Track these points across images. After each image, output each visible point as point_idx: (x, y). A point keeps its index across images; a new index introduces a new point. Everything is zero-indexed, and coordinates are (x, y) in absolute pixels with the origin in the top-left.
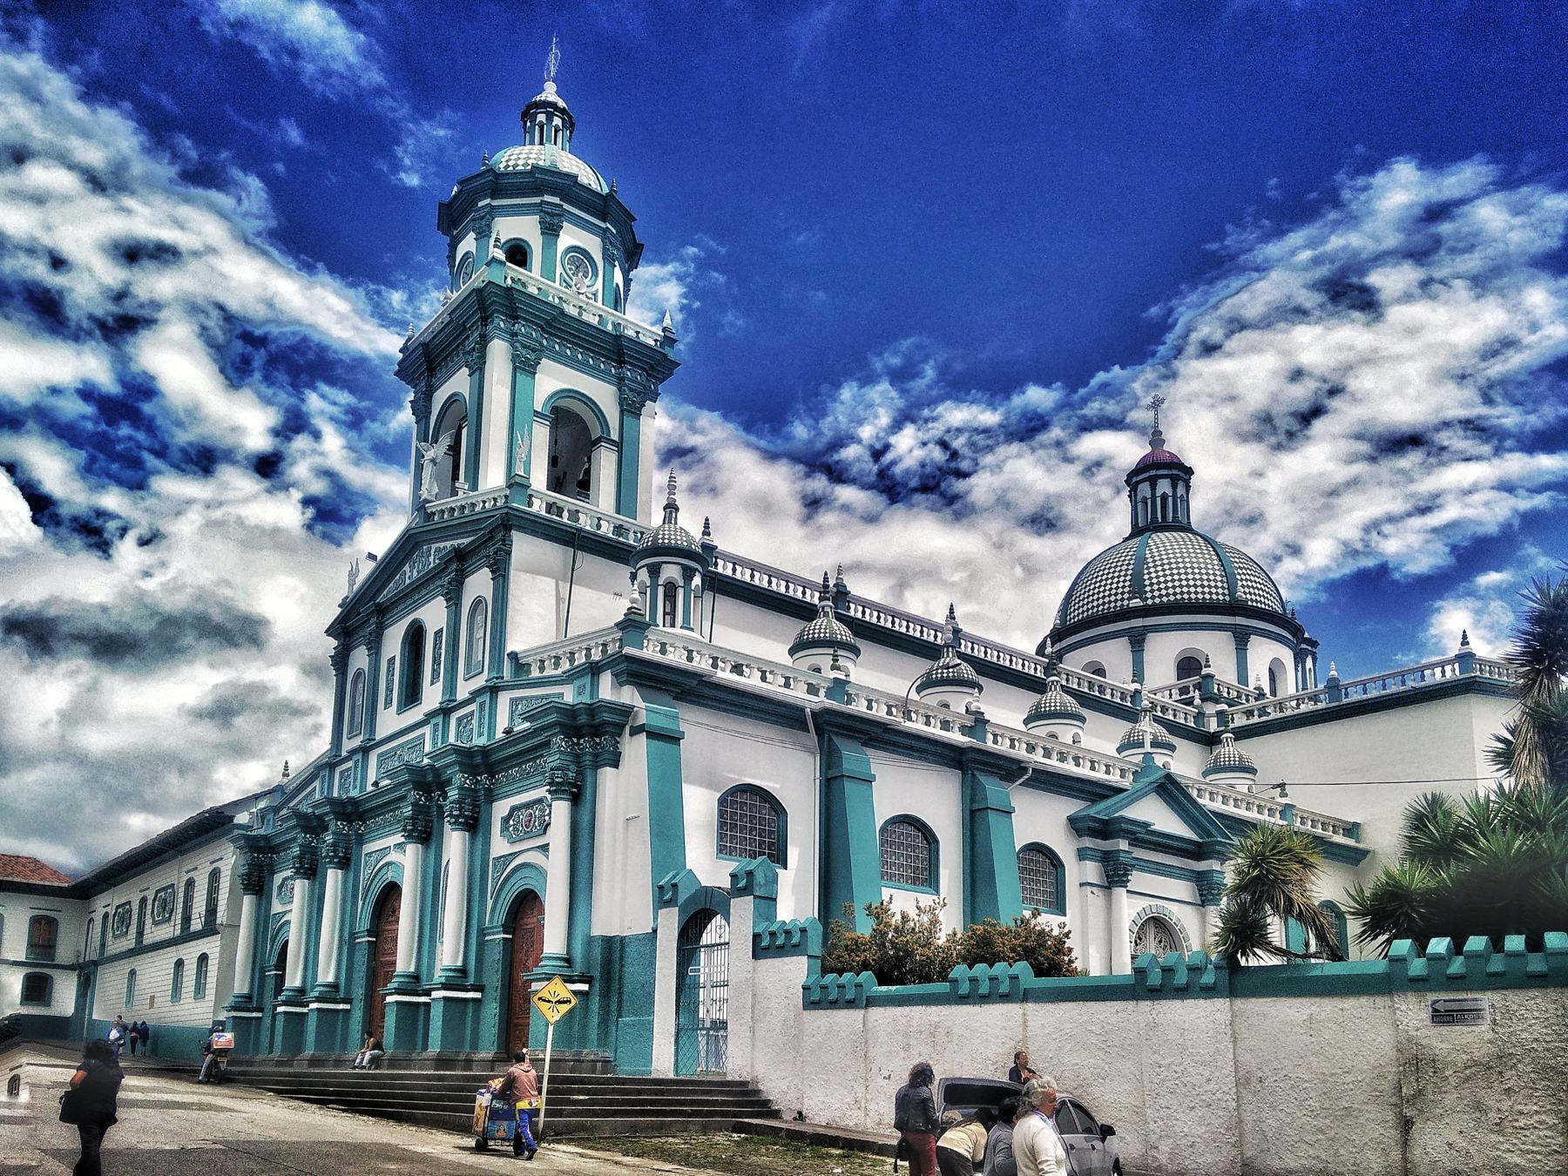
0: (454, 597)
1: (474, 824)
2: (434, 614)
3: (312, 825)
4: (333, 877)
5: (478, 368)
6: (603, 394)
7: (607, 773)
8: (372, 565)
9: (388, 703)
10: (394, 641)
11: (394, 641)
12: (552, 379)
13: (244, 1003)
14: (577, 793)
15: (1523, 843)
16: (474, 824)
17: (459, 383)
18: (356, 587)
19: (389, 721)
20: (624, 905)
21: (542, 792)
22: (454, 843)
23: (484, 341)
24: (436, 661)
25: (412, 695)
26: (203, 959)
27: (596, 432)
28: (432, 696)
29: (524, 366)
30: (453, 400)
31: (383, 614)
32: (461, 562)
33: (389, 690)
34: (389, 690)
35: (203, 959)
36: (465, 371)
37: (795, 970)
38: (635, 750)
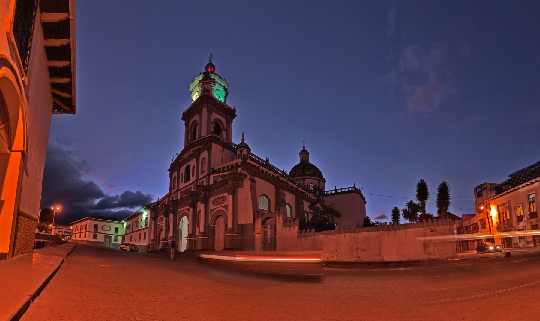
0: (198, 158)
1: (206, 202)
2: (193, 163)
3: (167, 206)
4: (171, 216)
5: (200, 113)
6: (223, 120)
7: (240, 189)
8: (177, 156)
9: (182, 181)
10: (183, 170)
11: (183, 170)
12: (215, 116)
13: (153, 240)
14: (234, 193)
15: (194, 224)
16: (206, 202)
17: (196, 117)
18: (174, 160)
19: (182, 185)
20: (246, 217)
21: (188, 207)
22: (201, 207)
23: (202, 108)
24: (193, 172)
25: (187, 179)
26: (145, 233)
27: (222, 128)
28: (192, 179)
29: (210, 113)
30: (195, 121)
31: (181, 165)
32: (199, 152)
33: (182, 179)
34: (182, 179)
35: (145, 233)
36: (197, 115)
37: (295, 230)
38: (247, 183)
